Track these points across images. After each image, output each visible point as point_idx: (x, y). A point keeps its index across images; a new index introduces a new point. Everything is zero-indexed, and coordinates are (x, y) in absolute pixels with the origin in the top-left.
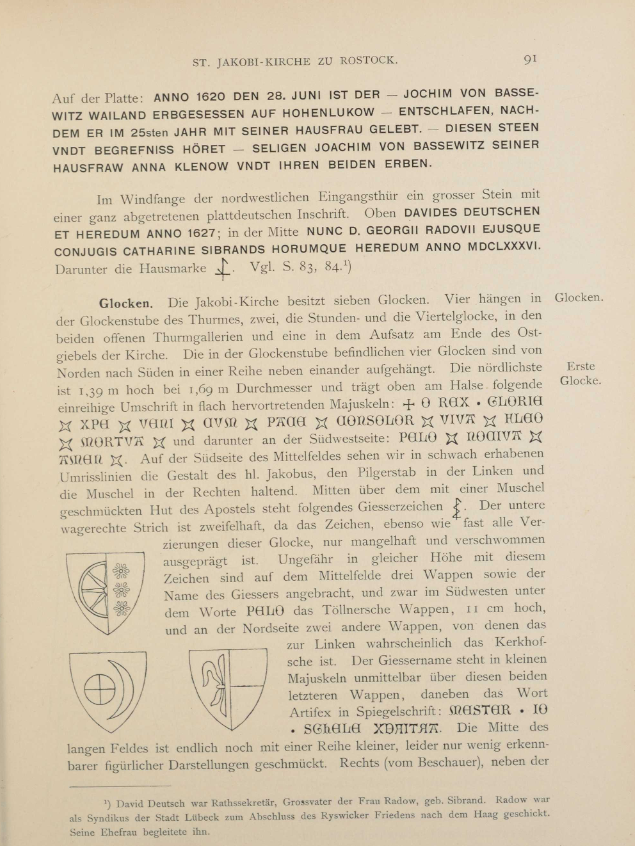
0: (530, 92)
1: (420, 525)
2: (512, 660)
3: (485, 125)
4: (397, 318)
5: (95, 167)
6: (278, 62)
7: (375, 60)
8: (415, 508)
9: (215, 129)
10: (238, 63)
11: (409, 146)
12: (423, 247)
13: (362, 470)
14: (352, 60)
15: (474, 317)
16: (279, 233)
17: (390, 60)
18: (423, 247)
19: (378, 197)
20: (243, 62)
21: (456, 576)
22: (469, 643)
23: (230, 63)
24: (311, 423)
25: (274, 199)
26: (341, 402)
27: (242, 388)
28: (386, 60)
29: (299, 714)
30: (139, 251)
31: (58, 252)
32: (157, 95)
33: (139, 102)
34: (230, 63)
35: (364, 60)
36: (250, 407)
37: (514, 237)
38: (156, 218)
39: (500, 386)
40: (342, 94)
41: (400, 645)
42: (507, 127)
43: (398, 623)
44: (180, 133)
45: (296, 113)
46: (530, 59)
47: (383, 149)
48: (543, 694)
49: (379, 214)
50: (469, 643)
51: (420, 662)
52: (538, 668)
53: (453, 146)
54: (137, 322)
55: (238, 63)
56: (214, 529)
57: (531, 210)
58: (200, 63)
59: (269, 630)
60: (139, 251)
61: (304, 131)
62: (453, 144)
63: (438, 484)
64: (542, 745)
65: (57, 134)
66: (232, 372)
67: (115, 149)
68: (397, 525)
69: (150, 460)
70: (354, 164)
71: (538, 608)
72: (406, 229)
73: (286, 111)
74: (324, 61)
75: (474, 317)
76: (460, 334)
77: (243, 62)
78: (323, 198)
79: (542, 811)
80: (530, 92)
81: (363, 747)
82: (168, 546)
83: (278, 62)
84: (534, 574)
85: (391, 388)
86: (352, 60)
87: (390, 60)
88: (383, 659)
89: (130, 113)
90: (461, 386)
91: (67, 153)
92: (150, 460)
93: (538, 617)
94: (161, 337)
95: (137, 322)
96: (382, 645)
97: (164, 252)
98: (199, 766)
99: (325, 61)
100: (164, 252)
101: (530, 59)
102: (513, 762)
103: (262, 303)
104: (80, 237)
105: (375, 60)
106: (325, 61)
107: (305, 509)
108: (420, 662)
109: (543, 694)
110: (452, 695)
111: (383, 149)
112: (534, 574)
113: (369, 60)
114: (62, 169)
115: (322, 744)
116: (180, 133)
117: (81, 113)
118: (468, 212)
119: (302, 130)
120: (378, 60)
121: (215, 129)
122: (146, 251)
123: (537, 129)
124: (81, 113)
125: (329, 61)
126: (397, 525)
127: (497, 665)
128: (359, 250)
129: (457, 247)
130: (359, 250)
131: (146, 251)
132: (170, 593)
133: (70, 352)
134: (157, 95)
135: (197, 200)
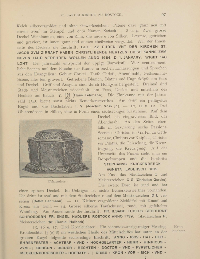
0: (22, 253)
3: (114, 46)
5: (51, 216)
6: (86, 15)
8: (116, 180)
11: (74, 52)
12: (111, 216)
14: (109, 15)
16: (113, 233)
18: (111, 216)
20: (75, 15)
21: (120, 159)
22: (121, 154)
23: (71, 15)
28: (119, 15)
30: (82, 253)
34: (71, 15)
35: (112, 15)
41: (99, 238)
44: (19, 53)
46: (163, 15)
47: (46, 59)
48: (60, 80)
50: (121, 154)
51: (93, 207)
53: (23, 58)
54: (163, 138)
55: (74, 15)
56: (88, 26)
58: (62, 15)
60: (82, 253)
70: (79, 217)
71: (165, 132)
72: (151, 57)
73: (129, 242)
76: (103, 227)
77: (75, 15)
78: (19, 107)
79: (138, 72)
80: (22, 253)
82: (135, 149)
83: (86, 15)
85: (70, 26)
86: (109, 15)
88: (159, 132)
94: (90, 232)
95: (163, 138)
99: (100, 15)
101: (163, 15)
105: (115, 15)
106: (100, 15)
107: (53, 238)
108: (93, 207)
109: (38, 42)
110: (79, 80)
111: (46, 59)
113: (114, 15)
116: (19, 53)
122: (83, 253)
123: (72, 53)
125: (102, 15)
127: (75, 197)
128: (110, 53)
129: (123, 237)
130: (110, 53)
131: (83, 253)
135: (162, 232)
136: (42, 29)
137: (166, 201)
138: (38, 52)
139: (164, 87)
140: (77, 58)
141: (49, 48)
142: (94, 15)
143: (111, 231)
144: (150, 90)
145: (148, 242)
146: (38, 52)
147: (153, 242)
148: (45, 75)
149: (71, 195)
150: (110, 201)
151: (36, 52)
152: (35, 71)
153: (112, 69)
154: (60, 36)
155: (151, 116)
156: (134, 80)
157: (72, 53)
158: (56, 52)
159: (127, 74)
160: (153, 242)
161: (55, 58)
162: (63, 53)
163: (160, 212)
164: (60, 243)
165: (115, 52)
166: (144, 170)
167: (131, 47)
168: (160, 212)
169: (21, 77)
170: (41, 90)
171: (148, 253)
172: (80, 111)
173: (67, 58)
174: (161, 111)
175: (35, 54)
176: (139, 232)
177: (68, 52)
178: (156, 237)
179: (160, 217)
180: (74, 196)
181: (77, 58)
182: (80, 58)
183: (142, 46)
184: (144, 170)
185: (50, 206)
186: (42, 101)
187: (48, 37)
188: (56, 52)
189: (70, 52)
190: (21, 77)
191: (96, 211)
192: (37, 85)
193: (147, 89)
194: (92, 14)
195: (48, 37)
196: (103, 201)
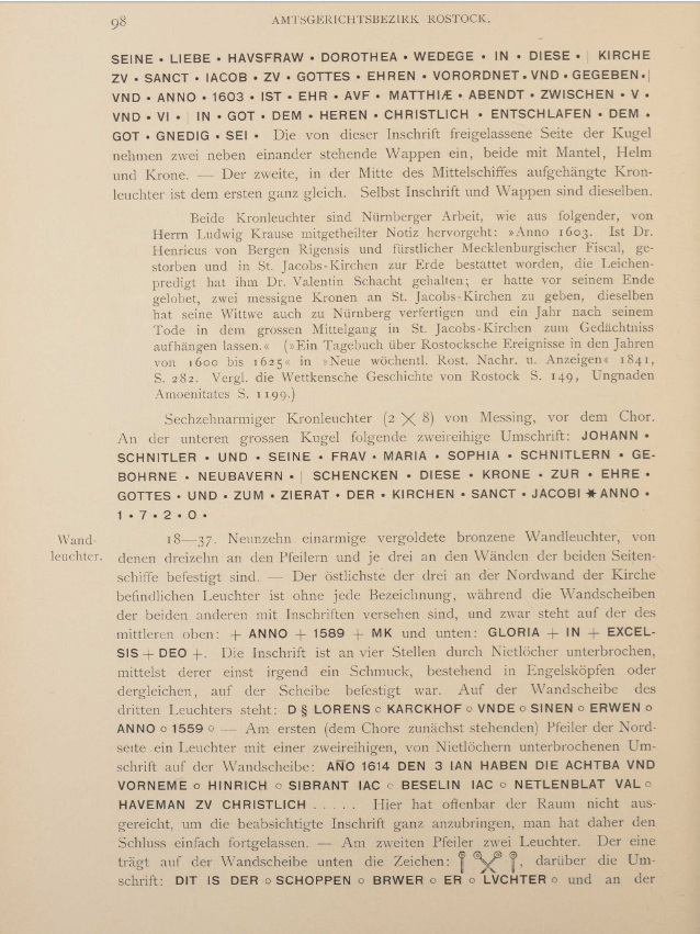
1: (631, 671)
2: (494, 249)
3: (634, 705)
7: (465, 19)
13: (551, 725)
14: (441, 19)
17: (481, 19)
19: (419, 250)
25: (419, 250)
27: (228, 174)
28: (478, 18)
30: (410, 95)
31: (227, 805)
35: (453, 19)
36: (445, 233)
37: (140, 833)
39: (359, 439)
42: (266, 804)
43: (571, 591)
45: (466, 75)
51: (502, 748)
56: (524, 266)
57: (350, 474)
60: (410, 95)
64: (647, 556)
65: (276, 116)
66: (616, 134)
67: (459, 55)
68: (125, 598)
81: (494, 249)
84: (641, 613)
86: (441, 19)
87: (481, 19)
90: (568, 154)
91: (128, 120)
93: (647, 604)
97: (403, 457)
98: (300, 730)
100: (403, 457)
102: (634, 192)
103: (487, 298)
105: (465, 19)
108: (502, 748)
112: (641, 613)
113: (458, 19)
115: (542, 801)
117: (553, 477)
121: (391, 92)
122: (368, 57)
124: (553, 477)
126: (125, 598)
131: (368, 57)
132: (234, 536)
136: (333, 550)
138: (637, 110)
141: (400, 438)
143: (563, 149)
144: (599, 653)
146: (637, 110)
147: (243, 786)
149: (504, 688)
150: (587, 557)
151: (120, 97)
152: (148, 164)
156: (495, 826)
157: (612, 97)
159: (387, 438)
160: (243, 786)
161: (376, 77)
162: (609, 436)
163: (268, 478)
165: (601, 708)
166: (301, 807)
167: (613, 113)
171: (512, 879)
174: (406, 174)
177: (620, 75)
183: (606, 55)
184: (301, 807)
185: (318, 476)
186: (565, 329)
189: (604, 93)
191: (450, 189)
192: (225, 330)
196: (397, 539)
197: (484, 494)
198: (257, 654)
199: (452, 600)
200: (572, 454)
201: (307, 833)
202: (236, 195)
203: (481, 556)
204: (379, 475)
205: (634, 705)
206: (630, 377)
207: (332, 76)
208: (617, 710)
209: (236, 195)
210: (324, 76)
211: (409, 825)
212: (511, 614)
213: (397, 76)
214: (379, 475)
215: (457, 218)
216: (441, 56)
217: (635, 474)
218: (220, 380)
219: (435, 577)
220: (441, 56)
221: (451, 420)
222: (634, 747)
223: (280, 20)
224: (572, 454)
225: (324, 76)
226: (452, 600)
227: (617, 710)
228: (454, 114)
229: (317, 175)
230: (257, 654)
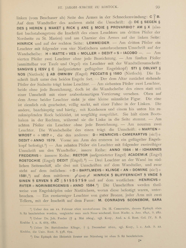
2: (61, 115)
3: (62, 186)
4: (59, 34)
7: (111, 7)
9: (96, 27)
10: (85, 7)
14: (105, 7)
15: (136, 74)
24: (81, 100)
26: (52, 38)
29: (31, 100)
32: (138, 26)
33: (159, 39)
35: (108, 7)
38: (50, 34)
40: (30, 135)
46: (158, 7)
49: (148, 94)
52: (22, 158)
53: (97, 170)
56: (49, 60)
58: (60, 8)
59: (25, 39)
61: (149, 150)
62: (97, 170)
63: (96, 103)
68: (20, 90)
69: (20, 24)
73: (18, 43)
74: (97, 7)
75: (136, 74)
78: (44, 196)
85: (30, 90)
86: (105, 7)
89: (84, 27)
90: (52, 39)
92: (20, 24)
96: (38, 34)
99: (97, 7)
101: (158, 7)
104: (31, 29)
105: (111, 7)
106: (97, 7)
108: (92, 191)
112: (67, 135)
113: (110, 7)
114: (149, 150)
118: (103, 53)
119: (148, 149)
120: (113, 7)
125: (98, 7)
126: (20, 90)
128: (18, 44)
132: (19, 38)
133: (39, 212)
134: (138, 26)
137: (77, 120)
138: (137, 149)
139: (158, 45)
140: (88, 53)
142: (90, 7)
144: (109, 48)
145: (45, 185)
146: (137, 149)
148: (76, 65)
153: (120, 84)
154: (91, 99)
155: (41, 17)
158: (140, 175)
163: (23, 136)
164: (139, 175)
168: (23, 136)
169: (21, 36)
170: (90, 236)
172: (85, 200)
173: (135, 149)
174: (127, 89)
175: (42, 181)
176: (37, 65)
178: (58, 160)
179: (81, 201)
180: (111, 180)
181: (88, 53)
182: (91, 53)
187: (68, 38)
188: (140, 175)
190: (21, 36)
193: (106, 47)
194: (89, 6)
195: (68, 38)
197: (83, 170)
198: (60, 79)
199: (76, 111)
200: (89, 170)
201: (106, 117)
202: (128, 94)
203: (102, 89)
204: (56, 28)
205: (62, 186)
206: (147, 208)
207: (62, 54)
208: (21, 136)
209: (128, 94)
210: (60, 54)
211: (23, 54)
212: (144, 145)
213: (37, 28)
214: (56, 28)
215: (56, 105)
216: (28, 156)
217: (63, 54)
218: (63, 141)
219: (51, 34)
220: (28, 156)
221: (63, 49)
222: (108, 22)
223: (69, 7)
224: (89, 170)
225: (60, 54)
226: (76, 111)
227: (21, 136)
228: (136, 175)
229: (34, 120)
230: (60, 79)
